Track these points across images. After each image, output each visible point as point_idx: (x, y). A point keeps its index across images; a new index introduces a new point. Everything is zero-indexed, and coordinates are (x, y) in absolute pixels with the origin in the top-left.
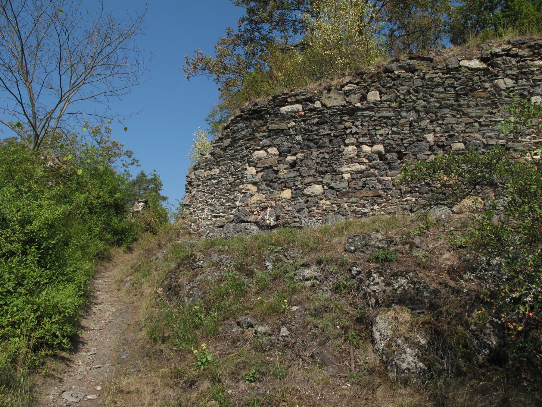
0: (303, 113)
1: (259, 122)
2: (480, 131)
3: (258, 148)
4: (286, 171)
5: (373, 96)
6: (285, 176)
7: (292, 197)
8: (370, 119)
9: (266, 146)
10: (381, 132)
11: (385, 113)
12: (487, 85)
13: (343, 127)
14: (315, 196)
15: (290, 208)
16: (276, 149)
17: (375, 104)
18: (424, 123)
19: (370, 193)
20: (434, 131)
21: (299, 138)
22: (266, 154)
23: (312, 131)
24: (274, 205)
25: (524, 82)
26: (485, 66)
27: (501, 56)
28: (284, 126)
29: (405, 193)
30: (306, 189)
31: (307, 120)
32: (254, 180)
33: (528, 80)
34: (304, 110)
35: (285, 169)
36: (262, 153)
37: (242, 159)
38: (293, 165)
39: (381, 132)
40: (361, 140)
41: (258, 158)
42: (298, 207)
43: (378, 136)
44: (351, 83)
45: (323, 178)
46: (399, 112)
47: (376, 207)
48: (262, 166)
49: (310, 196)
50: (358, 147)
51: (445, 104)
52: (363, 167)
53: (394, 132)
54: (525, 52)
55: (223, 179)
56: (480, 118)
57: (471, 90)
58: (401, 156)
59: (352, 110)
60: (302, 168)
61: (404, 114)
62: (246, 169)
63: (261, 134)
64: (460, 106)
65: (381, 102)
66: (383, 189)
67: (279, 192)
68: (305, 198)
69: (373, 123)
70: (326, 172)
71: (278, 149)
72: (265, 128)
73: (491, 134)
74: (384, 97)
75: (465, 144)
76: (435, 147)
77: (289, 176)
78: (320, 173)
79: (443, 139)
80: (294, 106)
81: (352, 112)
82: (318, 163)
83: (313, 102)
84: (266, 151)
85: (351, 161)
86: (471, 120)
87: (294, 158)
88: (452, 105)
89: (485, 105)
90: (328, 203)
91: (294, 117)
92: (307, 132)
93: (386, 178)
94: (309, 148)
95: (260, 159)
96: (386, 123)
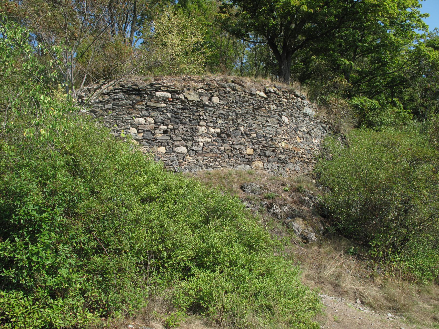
1: (138, 98)
2: (262, 129)
3: (139, 116)
4: (161, 135)
5: (216, 100)
6: (161, 138)
9: (145, 116)
10: (219, 122)
11: (221, 111)
12: (266, 106)
13: (198, 114)
14: (182, 153)
17: (217, 105)
18: (240, 121)
19: (214, 155)
22: (145, 121)
26: (265, 96)
27: (272, 93)
28: (159, 105)
29: (231, 157)
33: (281, 108)
34: (172, 98)
36: (142, 120)
37: (125, 121)
38: (165, 132)
39: (219, 122)
40: (209, 124)
42: (171, 159)
44: (202, 88)
45: (187, 143)
46: (228, 112)
47: (217, 163)
49: (179, 153)
50: (207, 128)
52: (210, 140)
53: (226, 123)
54: (281, 93)
56: (263, 122)
57: (260, 107)
59: (204, 105)
61: (231, 114)
62: (129, 129)
63: (140, 107)
64: (255, 114)
66: (219, 153)
68: (176, 154)
69: (216, 116)
70: (189, 140)
71: (154, 120)
73: (267, 131)
74: (222, 102)
75: (256, 134)
76: (244, 134)
77: (163, 138)
78: (184, 140)
79: (248, 130)
80: (164, 93)
81: (204, 106)
82: (183, 134)
83: (179, 94)
84: (145, 119)
85: (203, 135)
86: (260, 123)
87: (166, 127)
88: (252, 113)
89: (265, 116)
90: (191, 158)
92: (174, 112)
96: (222, 117)
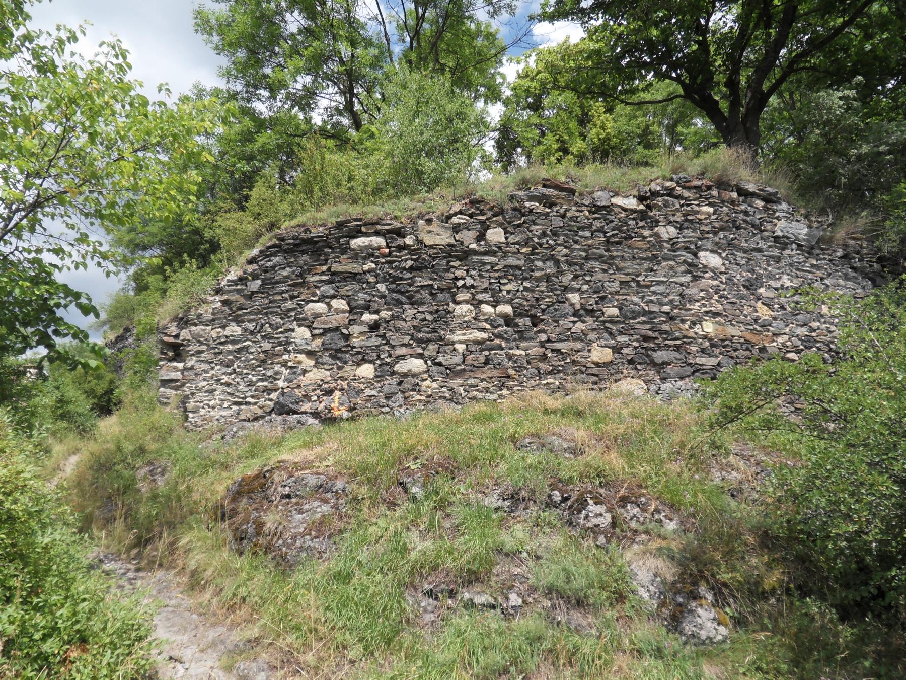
0: (387, 251)
5: (495, 235)
7: (376, 376)
8: (492, 267)
9: (327, 297)
10: (509, 287)
11: (512, 261)
13: (452, 276)
15: (374, 393)
18: (566, 279)
19: (496, 373)
20: (579, 289)
23: (401, 279)
30: (398, 365)
31: (395, 262)
34: (388, 247)
36: (320, 307)
37: (285, 314)
38: (374, 327)
39: (509, 287)
40: (480, 297)
42: (386, 389)
44: (460, 212)
48: (322, 326)
51: (594, 254)
53: (526, 289)
55: (250, 343)
56: (638, 276)
57: (625, 238)
59: (465, 252)
60: (390, 334)
61: (539, 264)
62: (293, 330)
63: (317, 278)
64: (612, 257)
65: (507, 244)
69: (497, 274)
70: (429, 341)
73: (652, 298)
77: (368, 343)
81: (465, 255)
84: (328, 304)
86: (628, 278)
87: (375, 317)
88: (601, 256)
90: (435, 385)
93: (518, 352)
95: (317, 316)
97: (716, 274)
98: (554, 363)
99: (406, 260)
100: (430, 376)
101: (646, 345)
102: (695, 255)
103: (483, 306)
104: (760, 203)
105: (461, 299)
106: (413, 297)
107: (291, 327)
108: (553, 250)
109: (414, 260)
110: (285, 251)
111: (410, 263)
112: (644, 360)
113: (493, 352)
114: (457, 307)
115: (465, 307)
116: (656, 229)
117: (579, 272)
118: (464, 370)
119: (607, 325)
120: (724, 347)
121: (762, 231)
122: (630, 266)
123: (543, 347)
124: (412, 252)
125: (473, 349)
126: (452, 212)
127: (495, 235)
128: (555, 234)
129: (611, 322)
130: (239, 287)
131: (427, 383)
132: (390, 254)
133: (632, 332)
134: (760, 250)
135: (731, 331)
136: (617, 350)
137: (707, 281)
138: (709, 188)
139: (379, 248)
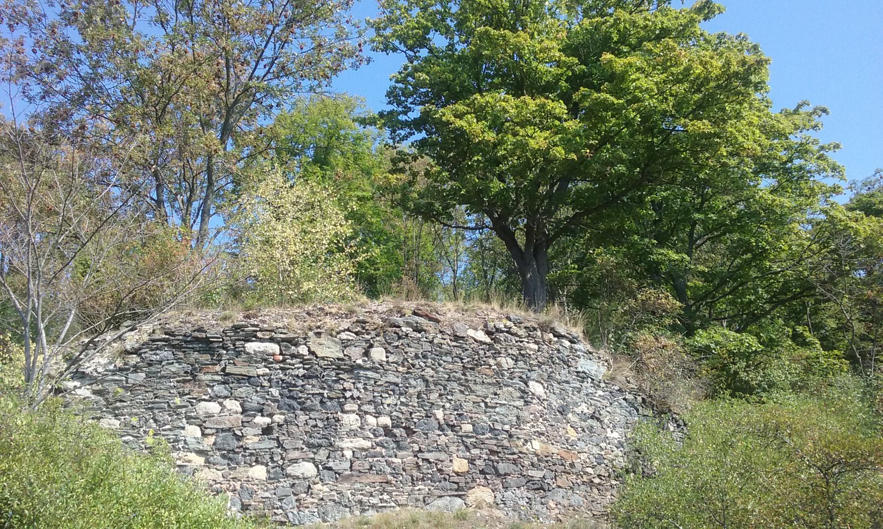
0: (281, 358)
1: (205, 358)
2: (486, 412)
3: (204, 397)
4: (256, 439)
5: (378, 354)
6: (257, 446)
7: (270, 478)
8: (375, 382)
9: (220, 397)
10: (389, 401)
11: (392, 378)
12: (492, 362)
13: (341, 387)
14: (304, 479)
15: (267, 494)
16: (238, 403)
17: (381, 365)
18: (434, 396)
19: (378, 479)
20: (443, 406)
21: (275, 392)
23: (295, 386)
24: (238, 488)
25: (521, 364)
27: (502, 332)
28: (253, 372)
30: (290, 468)
31: (288, 369)
32: (201, 448)
33: (525, 363)
34: (281, 354)
35: (255, 435)
36: (213, 407)
37: (174, 410)
38: (267, 431)
39: (389, 401)
40: (365, 408)
41: (206, 413)
42: (279, 492)
43: (386, 406)
44: (348, 330)
45: (315, 453)
46: (407, 379)
47: (386, 497)
48: (215, 426)
49: (298, 478)
50: (361, 417)
51: (454, 376)
53: (402, 403)
55: (131, 438)
56: (485, 398)
57: (476, 365)
58: (410, 432)
59: (352, 366)
60: (284, 438)
61: (413, 382)
62: (183, 428)
63: (209, 377)
64: (467, 381)
65: (387, 362)
66: (391, 474)
67: (246, 469)
69: (380, 389)
70: (320, 446)
72: (218, 368)
73: (497, 418)
75: (474, 425)
77: (262, 446)
79: (453, 418)
81: (353, 369)
82: (306, 432)
84: (221, 404)
86: (479, 399)
87: (268, 420)
88: (460, 379)
90: (325, 488)
91: (265, 360)
93: (394, 460)
94: (291, 408)
95: (210, 416)
96: (393, 390)
97: (541, 400)
98: (424, 471)
99: (299, 368)
100: (321, 479)
101: (493, 458)
102: (526, 383)
103: (368, 416)
104: (567, 343)
105: (349, 409)
106: (304, 403)
107: (180, 424)
108: (423, 370)
109: (307, 369)
110: (174, 346)
111: (302, 372)
112: (490, 472)
113: (375, 459)
114: (345, 416)
115: (353, 417)
116: (499, 359)
117: (443, 392)
118: (352, 475)
119: (464, 439)
120: (547, 462)
121: (569, 367)
122: (480, 389)
123: (415, 456)
124: (304, 362)
125: (359, 456)
126: (341, 328)
127: (378, 354)
128: (425, 357)
129: (467, 437)
130: (116, 378)
131: (319, 486)
132: (283, 361)
133: (482, 446)
134: (568, 382)
135: (553, 449)
136: (471, 461)
137: (536, 407)
138: (535, 329)
139: (274, 355)
